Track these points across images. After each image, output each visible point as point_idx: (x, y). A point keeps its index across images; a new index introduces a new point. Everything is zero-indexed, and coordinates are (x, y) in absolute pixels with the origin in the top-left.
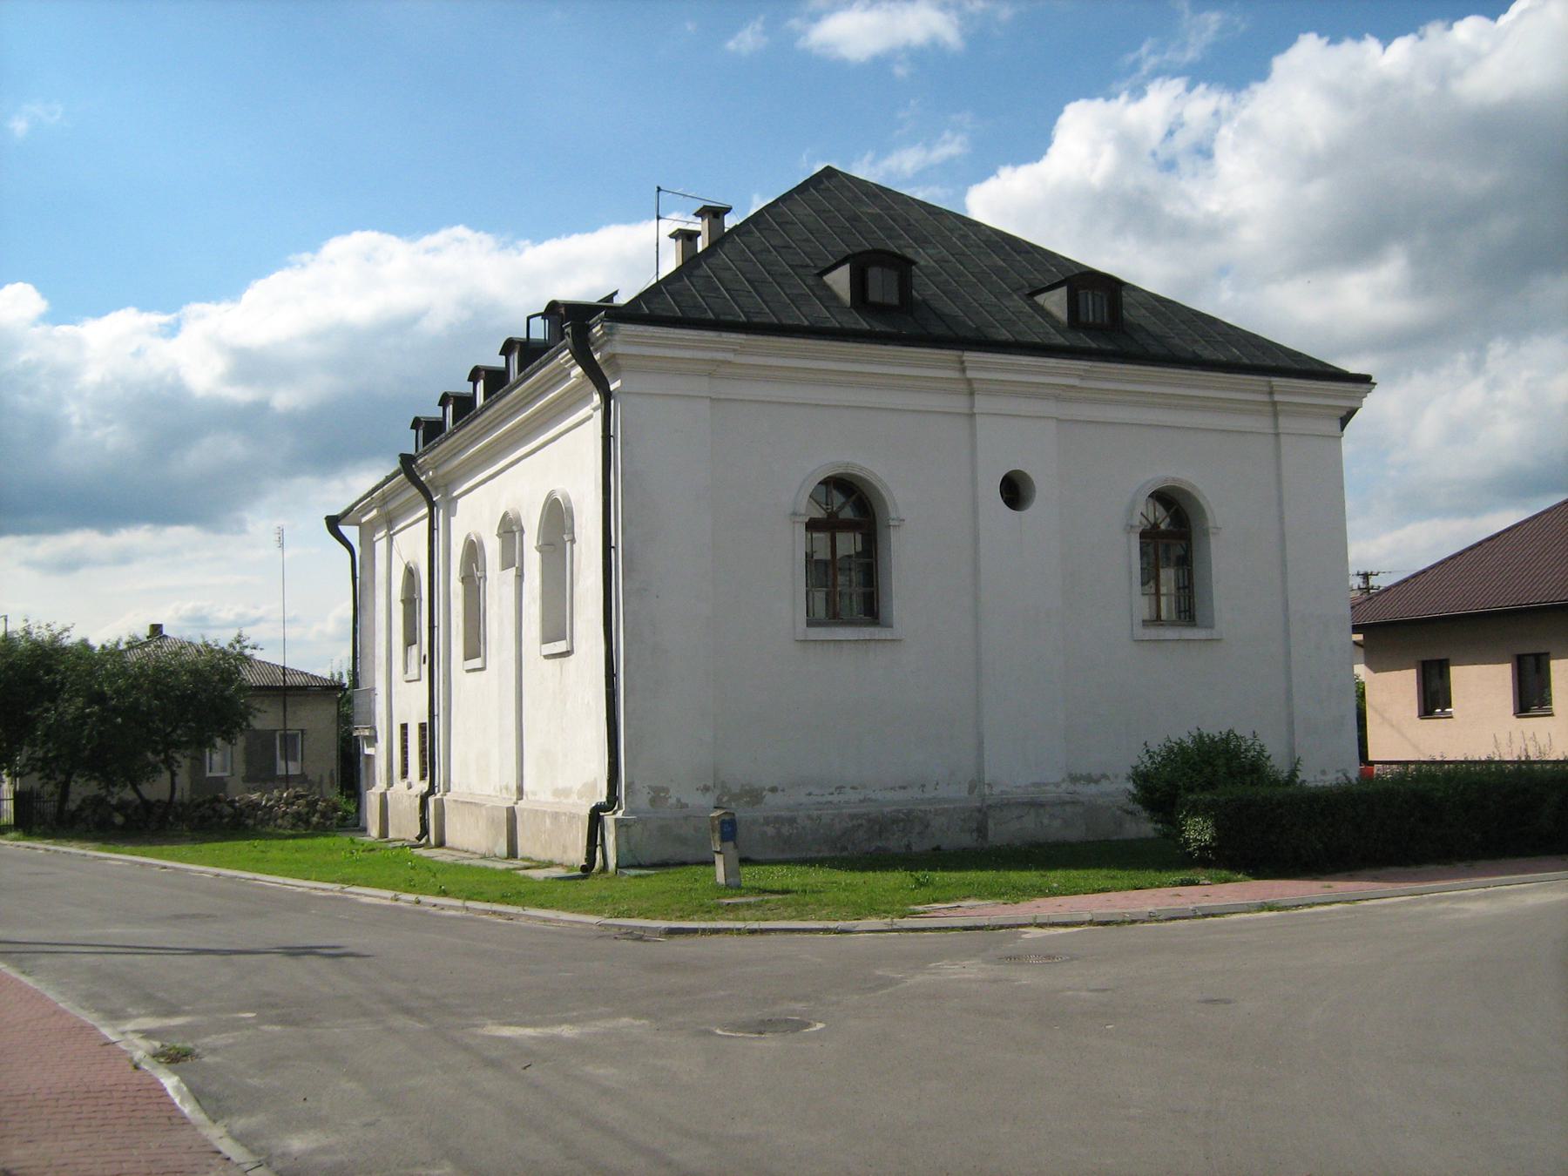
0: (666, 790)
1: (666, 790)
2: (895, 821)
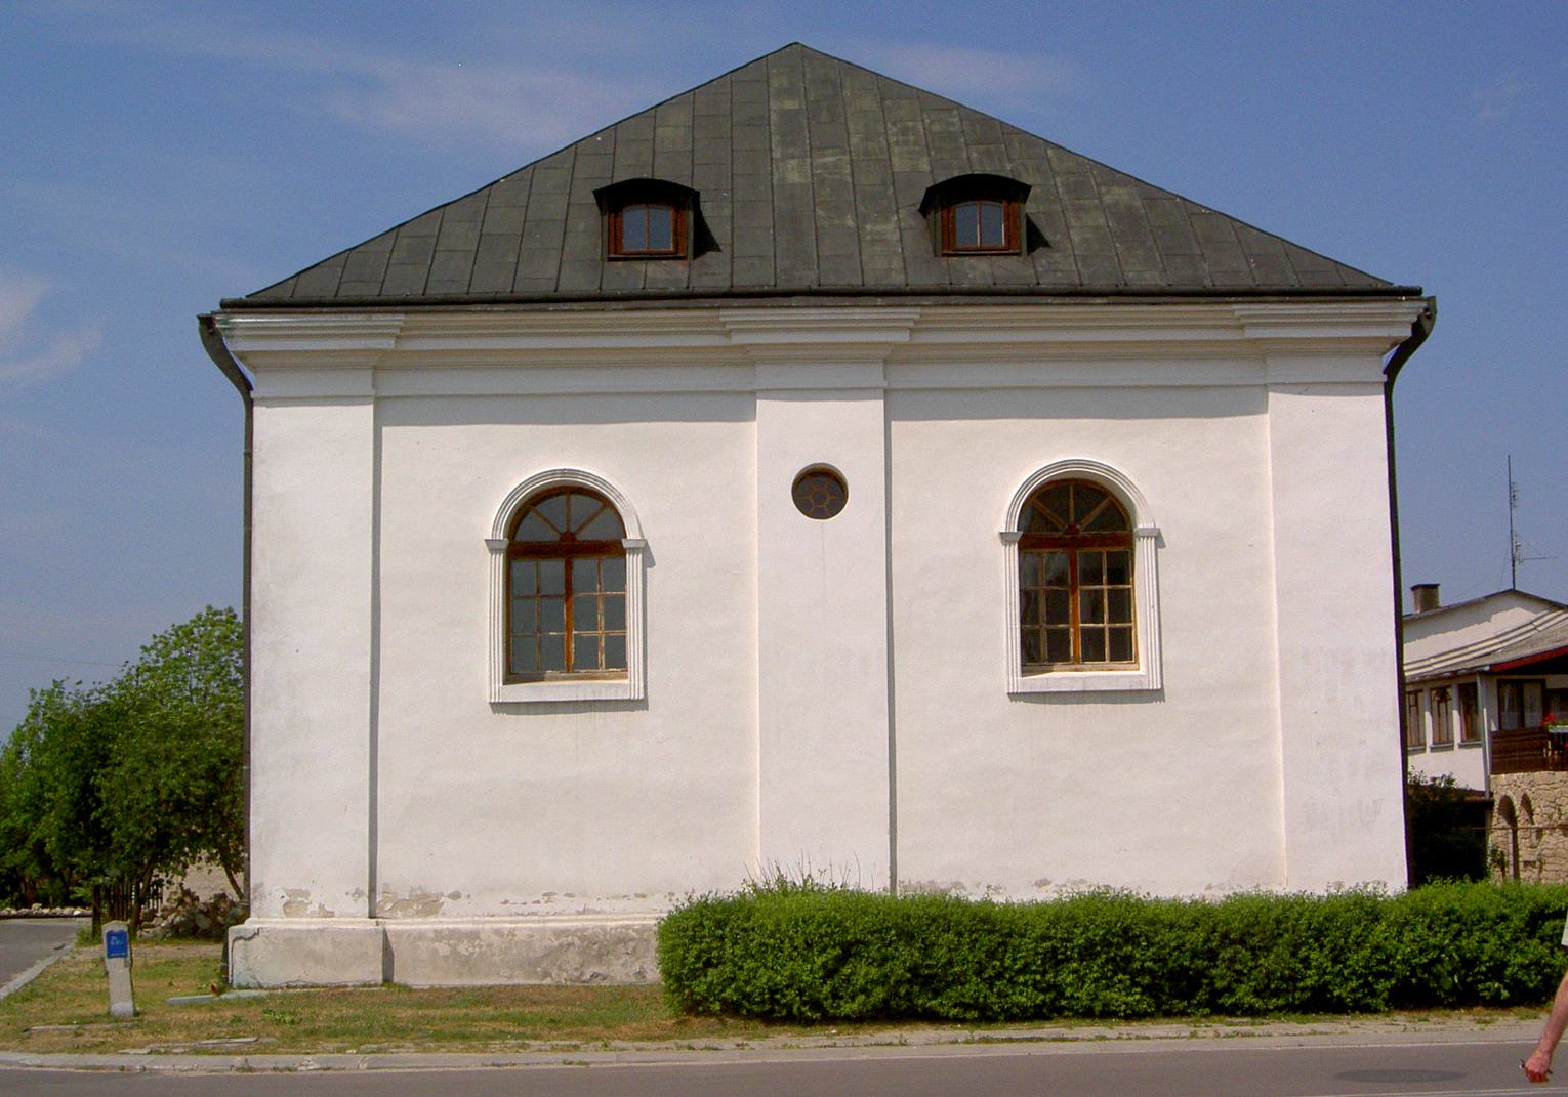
0: (306, 894)
1: (306, 894)
2: (623, 940)
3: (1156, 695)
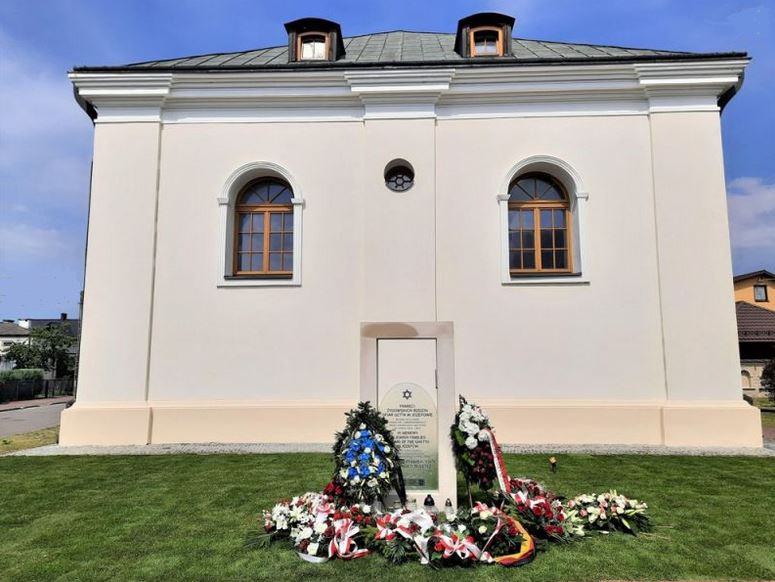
3: (299, 286)
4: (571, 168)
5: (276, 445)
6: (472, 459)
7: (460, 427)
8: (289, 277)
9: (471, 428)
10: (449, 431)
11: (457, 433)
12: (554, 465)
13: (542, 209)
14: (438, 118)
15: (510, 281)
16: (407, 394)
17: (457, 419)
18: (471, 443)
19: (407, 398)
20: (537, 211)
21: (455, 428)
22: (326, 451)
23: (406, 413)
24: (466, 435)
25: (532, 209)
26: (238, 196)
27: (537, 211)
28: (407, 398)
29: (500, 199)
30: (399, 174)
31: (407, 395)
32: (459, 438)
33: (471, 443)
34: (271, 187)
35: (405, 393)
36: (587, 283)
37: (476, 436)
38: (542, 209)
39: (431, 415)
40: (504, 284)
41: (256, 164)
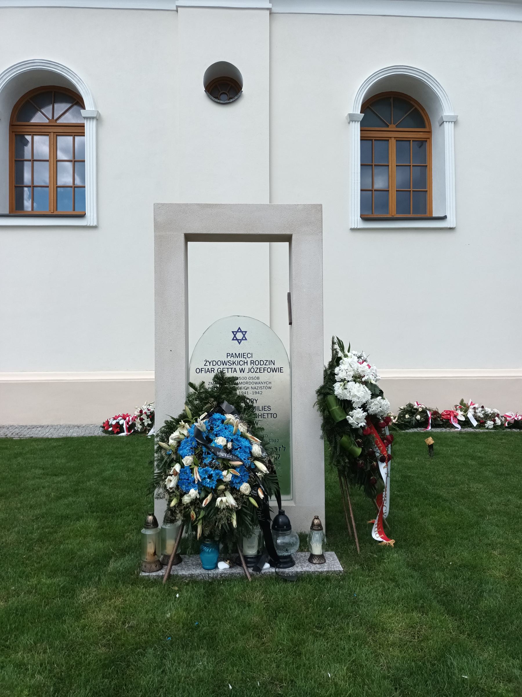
4: (438, 84)
5: (69, 427)
6: (359, 445)
7: (338, 388)
8: (82, 216)
9: (358, 393)
10: (313, 397)
11: (330, 398)
12: (431, 446)
13: (398, 140)
14: (275, 10)
15: (361, 224)
16: (239, 335)
17: (330, 377)
18: (357, 418)
19: (239, 341)
20: (393, 143)
21: (325, 392)
22: (96, 434)
23: (238, 367)
24: (347, 405)
25: (386, 140)
26: (14, 107)
27: (393, 143)
28: (239, 341)
29: (351, 118)
30: (223, 85)
31: (239, 336)
32: (335, 408)
33: (357, 418)
34: (56, 105)
35: (244, 333)
36: (451, 229)
37: (364, 407)
38: (398, 140)
39: (280, 370)
40: (353, 230)
41: (33, 62)
